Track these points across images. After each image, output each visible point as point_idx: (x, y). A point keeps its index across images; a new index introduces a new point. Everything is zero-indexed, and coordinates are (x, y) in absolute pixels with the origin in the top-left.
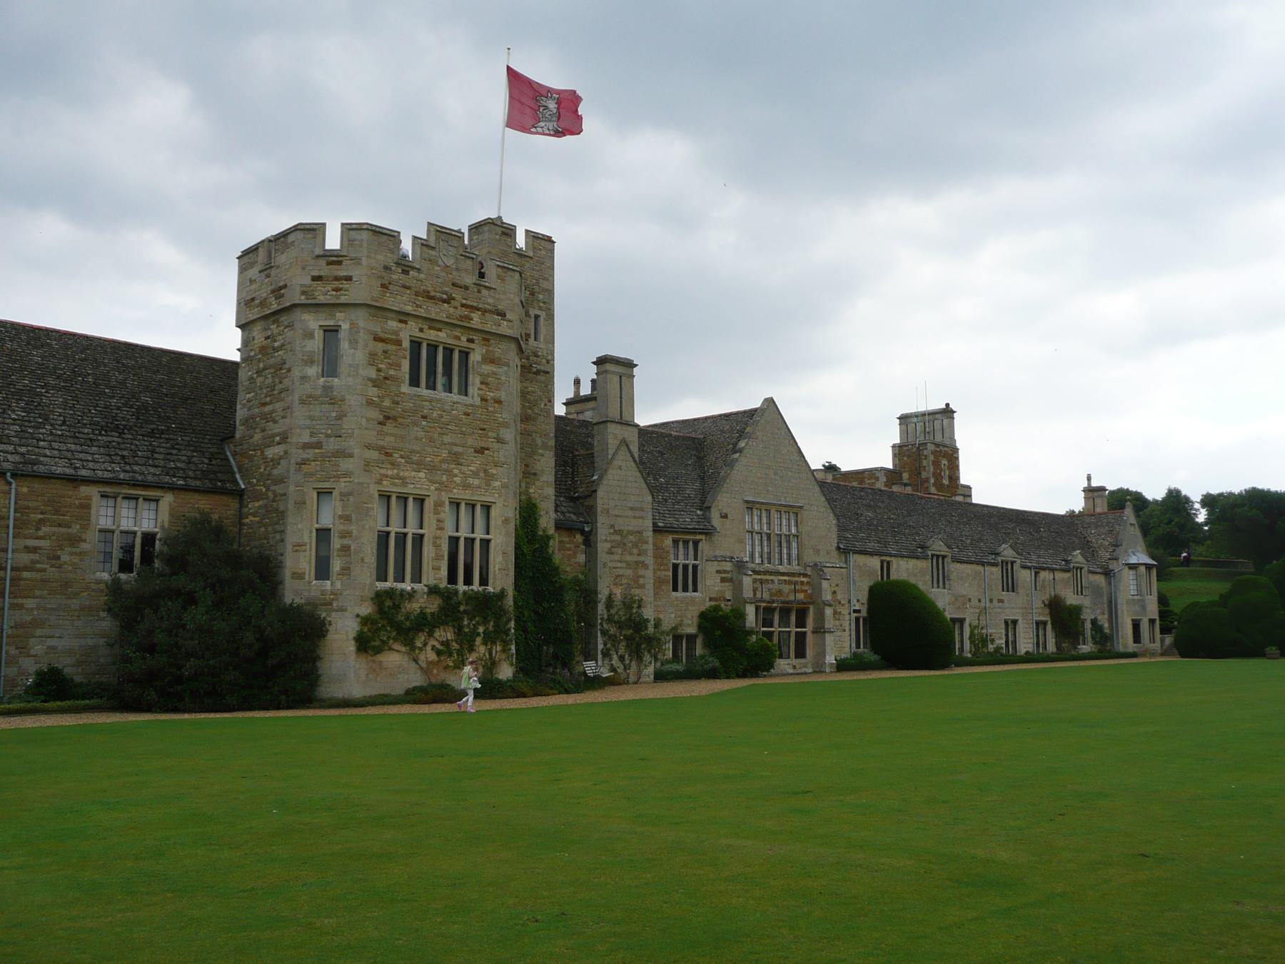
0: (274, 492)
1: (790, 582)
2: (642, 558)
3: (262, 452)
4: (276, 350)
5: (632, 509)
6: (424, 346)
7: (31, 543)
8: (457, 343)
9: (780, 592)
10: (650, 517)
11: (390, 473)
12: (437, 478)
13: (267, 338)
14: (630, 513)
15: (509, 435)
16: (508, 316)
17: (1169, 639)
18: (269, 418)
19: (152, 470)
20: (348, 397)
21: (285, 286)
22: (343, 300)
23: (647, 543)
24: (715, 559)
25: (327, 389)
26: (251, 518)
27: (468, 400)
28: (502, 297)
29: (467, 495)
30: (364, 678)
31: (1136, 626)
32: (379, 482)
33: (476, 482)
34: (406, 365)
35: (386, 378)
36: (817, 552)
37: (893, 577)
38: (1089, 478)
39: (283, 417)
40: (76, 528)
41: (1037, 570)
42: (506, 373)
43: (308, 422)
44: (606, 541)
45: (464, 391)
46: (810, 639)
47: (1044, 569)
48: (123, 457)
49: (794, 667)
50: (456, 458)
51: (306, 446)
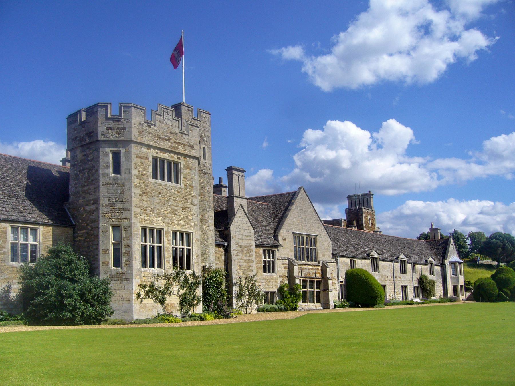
0: (91, 226)
1: (312, 269)
2: (251, 258)
3: (84, 208)
4: (89, 161)
5: (246, 236)
8: (172, 159)
9: (309, 273)
10: (254, 240)
11: (146, 218)
13: (83, 156)
14: (245, 238)
15: (196, 201)
16: (195, 148)
17: (468, 294)
18: (88, 192)
19: (33, 215)
20: (125, 183)
21: (93, 132)
22: (122, 138)
24: (281, 259)
25: (115, 179)
26: (79, 238)
27: (179, 186)
28: (192, 139)
29: (180, 229)
30: (138, 311)
31: (455, 288)
33: (183, 223)
34: (151, 169)
35: (142, 175)
36: (324, 256)
37: (357, 267)
38: (432, 225)
39: (94, 192)
41: (414, 264)
43: (107, 194)
44: (235, 250)
45: (177, 181)
46: (322, 294)
47: (417, 264)
48: (19, 209)
49: (316, 306)
50: (174, 212)
51: (106, 205)
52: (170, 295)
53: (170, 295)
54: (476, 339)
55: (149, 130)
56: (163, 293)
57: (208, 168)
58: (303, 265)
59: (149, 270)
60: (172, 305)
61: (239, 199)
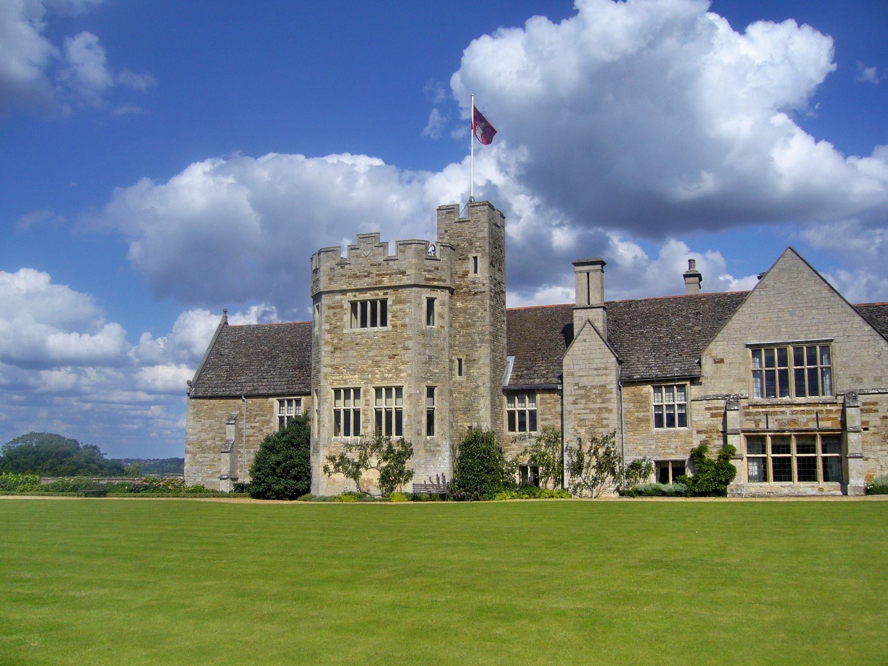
1: (808, 412)
2: (605, 405)
5: (595, 369)
6: (379, 303)
7: (253, 425)
12: (365, 377)
14: (595, 372)
23: (611, 393)
32: (332, 384)
33: (390, 375)
40: (268, 417)
42: (409, 307)
44: (571, 395)
50: (377, 364)
52: (367, 469)
53: (367, 469)
54: (341, 552)
55: (343, 272)
56: (358, 466)
57: (481, 285)
58: (773, 405)
59: (342, 437)
60: (369, 481)
61: (585, 311)
